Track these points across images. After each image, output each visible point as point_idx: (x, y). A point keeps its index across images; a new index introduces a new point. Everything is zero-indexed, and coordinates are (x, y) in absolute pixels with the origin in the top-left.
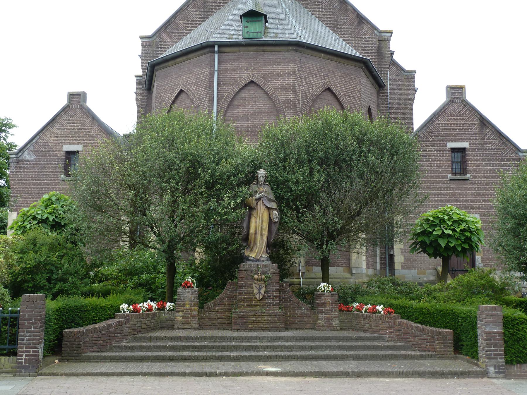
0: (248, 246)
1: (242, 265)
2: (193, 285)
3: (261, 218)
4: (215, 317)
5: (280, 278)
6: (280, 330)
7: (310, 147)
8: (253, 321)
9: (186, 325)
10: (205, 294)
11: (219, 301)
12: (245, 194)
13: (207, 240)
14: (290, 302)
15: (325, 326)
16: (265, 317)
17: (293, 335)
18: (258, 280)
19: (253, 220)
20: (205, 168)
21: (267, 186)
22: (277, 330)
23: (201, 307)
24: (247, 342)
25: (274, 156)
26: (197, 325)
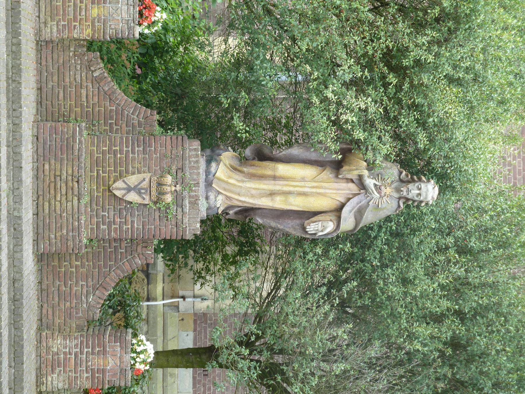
0: (243, 160)
1: (196, 144)
2: (145, 24)
3: (314, 190)
4: (67, 80)
5: (165, 240)
6: (36, 242)
7: (498, 314)
8: (58, 173)
9: (48, 9)
10: (124, 57)
11: (106, 89)
12: (374, 149)
13: (258, 56)
14: (105, 266)
15: (48, 353)
16: (69, 204)
17: (26, 273)
18: (160, 184)
19: (309, 171)
20: (440, 46)
21: (395, 204)
22: (37, 233)
23: (90, 45)
24: (8, 158)
25: (471, 222)
26: (48, 37)
